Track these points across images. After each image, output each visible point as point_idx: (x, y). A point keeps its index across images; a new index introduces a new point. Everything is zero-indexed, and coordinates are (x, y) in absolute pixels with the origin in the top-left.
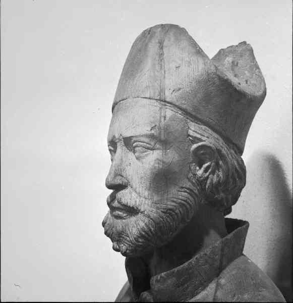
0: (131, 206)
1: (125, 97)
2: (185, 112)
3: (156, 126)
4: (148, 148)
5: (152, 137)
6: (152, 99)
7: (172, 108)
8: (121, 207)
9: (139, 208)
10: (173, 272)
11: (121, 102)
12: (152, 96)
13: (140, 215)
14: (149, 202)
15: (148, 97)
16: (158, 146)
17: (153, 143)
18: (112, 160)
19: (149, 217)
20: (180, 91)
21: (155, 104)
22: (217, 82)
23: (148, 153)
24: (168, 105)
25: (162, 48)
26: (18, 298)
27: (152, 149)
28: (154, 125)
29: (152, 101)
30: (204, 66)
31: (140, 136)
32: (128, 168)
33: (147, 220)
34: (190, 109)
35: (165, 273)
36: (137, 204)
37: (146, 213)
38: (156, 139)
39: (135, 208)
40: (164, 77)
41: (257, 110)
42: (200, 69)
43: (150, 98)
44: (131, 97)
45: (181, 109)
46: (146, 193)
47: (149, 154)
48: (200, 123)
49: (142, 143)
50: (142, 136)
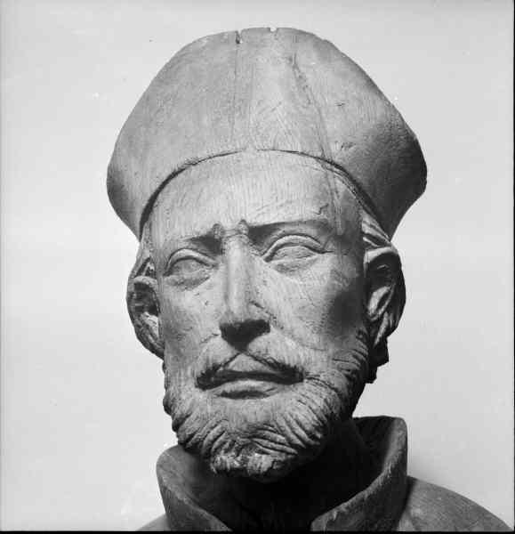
0: (292, 365)
1: (231, 148)
2: (359, 190)
3: (327, 205)
4: (315, 250)
5: (324, 227)
6: (307, 155)
7: (342, 178)
8: (267, 369)
9: (307, 369)
10: (363, 500)
11: (217, 158)
12: (307, 150)
13: (306, 385)
14: (324, 356)
15: (300, 151)
16: (331, 246)
17: (323, 239)
18: (323, 253)
19: (330, 386)
20: (352, 148)
21: (315, 167)
22: (403, 145)
23: (314, 257)
24: (335, 169)
25: (295, 67)
26: (501, 515)
27: (322, 252)
28: (324, 204)
29: (306, 158)
30: (383, 110)
31: (300, 222)
32: (262, 289)
33: (325, 393)
34: (365, 184)
35: (346, 504)
36: (303, 361)
37: (322, 378)
38: (330, 232)
39: (300, 369)
40: (321, 118)
41: (410, 206)
42: (378, 115)
43: (302, 154)
44: (250, 149)
45: (354, 181)
46: (315, 339)
47: (315, 261)
48: (369, 210)
49: (303, 238)
50: (305, 222)
